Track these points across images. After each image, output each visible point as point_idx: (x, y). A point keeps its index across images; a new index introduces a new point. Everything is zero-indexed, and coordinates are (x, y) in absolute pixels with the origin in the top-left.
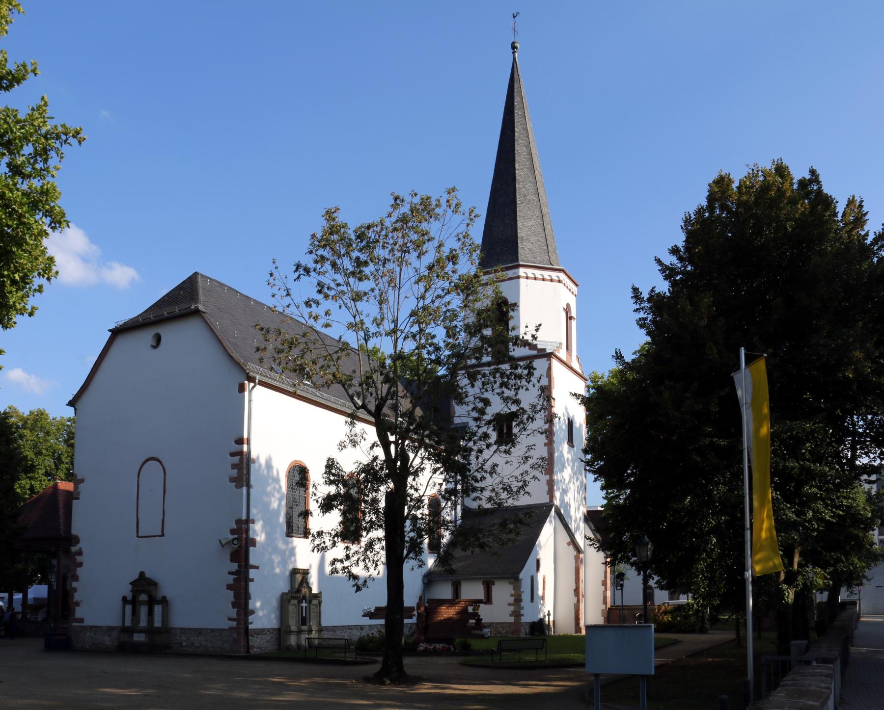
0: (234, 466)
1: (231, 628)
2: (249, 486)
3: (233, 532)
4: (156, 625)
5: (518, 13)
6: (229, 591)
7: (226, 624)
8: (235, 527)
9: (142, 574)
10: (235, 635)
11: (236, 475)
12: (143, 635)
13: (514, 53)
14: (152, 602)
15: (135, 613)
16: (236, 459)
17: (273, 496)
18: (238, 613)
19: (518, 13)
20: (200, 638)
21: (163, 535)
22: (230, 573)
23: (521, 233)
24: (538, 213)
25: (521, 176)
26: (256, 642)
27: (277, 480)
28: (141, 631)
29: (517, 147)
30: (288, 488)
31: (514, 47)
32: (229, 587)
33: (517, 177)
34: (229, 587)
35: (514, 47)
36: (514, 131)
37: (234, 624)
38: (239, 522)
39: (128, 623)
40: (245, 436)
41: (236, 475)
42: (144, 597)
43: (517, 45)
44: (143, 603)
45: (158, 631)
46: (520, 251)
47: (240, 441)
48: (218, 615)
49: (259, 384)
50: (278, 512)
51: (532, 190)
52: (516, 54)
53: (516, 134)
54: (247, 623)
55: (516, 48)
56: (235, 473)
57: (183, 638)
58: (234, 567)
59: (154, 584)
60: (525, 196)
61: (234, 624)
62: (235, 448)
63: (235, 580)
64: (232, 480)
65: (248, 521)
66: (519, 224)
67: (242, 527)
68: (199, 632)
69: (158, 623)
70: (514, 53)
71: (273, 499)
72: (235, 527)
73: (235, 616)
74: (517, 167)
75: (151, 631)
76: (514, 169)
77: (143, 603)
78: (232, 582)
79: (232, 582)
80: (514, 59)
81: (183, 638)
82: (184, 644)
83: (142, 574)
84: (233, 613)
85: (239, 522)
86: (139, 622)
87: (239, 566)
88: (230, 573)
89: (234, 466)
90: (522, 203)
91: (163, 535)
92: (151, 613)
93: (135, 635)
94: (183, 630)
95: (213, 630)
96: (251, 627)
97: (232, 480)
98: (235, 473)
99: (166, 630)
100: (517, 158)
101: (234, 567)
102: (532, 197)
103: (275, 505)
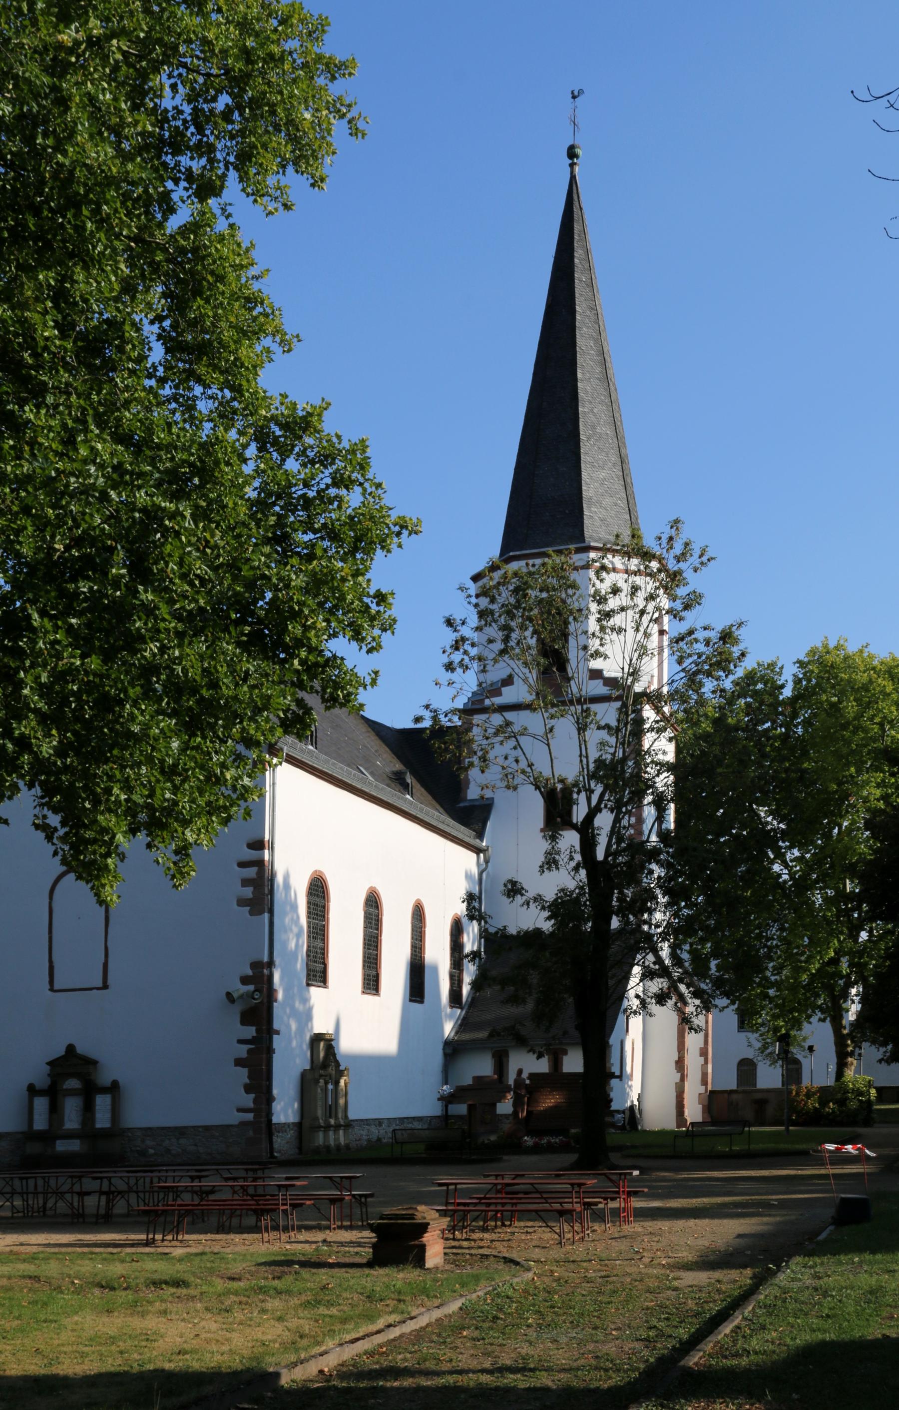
0: (245, 882)
1: (243, 1124)
2: (271, 912)
3: (245, 980)
4: (98, 1125)
5: (581, 92)
6: (238, 1068)
7: (235, 1118)
8: (250, 972)
9: (71, 1049)
10: (251, 1133)
11: (250, 896)
12: (77, 1142)
13: (572, 165)
14: (90, 1092)
15: (55, 1109)
16: (251, 872)
17: (291, 930)
18: (255, 1101)
19: (581, 92)
20: (183, 1141)
21: (105, 986)
22: (240, 1042)
23: (588, 491)
24: (615, 458)
25: (586, 392)
26: (283, 1143)
27: (294, 907)
28: (70, 1135)
29: (580, 341)
30: (309, 917)
31: (572, 153)
32: (239, 1062)
33: (581, 394)
34: (239, 1062)
35: (572, 153)
36: (573, 312)
37: (250, 1116)
38: (257, 966)
39: (40, 1123)
40: (267, 837)
41: (250, 896)
42: (73, 1083)
43: (579, 151)
44: (72, 1092)
45: (105, 1134)
46: (587, 522)
47: (258, 845)
48: (221, 1102)
49: (287, 761)
50: (295, 955)
51: (605, 417)
52: (577, 169)
53: (578, 317)
54: (269, 1113)
55: (577, 156)
56: (248, 892)
57: (149, 1142)
58: (250, 1032)
59: (91, 1063)
60: (593, 427)
61: (250, 1116)
62: (252, 855)
63: (249, 1051)
64: (242, 902)
65: (271, 964)
66: (584, 475)
67: (260, 976)
68: (181, 1132)
69: (102, 1120)
70: (572, 165)
71: (291, 936)
72: (250, 972)
73: (251, 1105)
74: (579, 375)
75: (88, 1133)
76: (575, 380)
77: (72, 1092)
78: (244, 1055)
79: (244, 1055)
80: (573, 178)
81: (149, 1142)
82: (151, 1151)
83: (71, 1049)
84: (248, 1100)
85: (257, 966)
86: (61, 1122)
87: (257, 1031)
88: (240, 1042)
89: (245, 882)
90: (589, 439)
91: (105, 986)
92: (88, 1108)
93: (58, 1142)
94: (149, 1132)
95: (207, 1128)
96: (275, 1120)
97: (242, 902)
98: (248, 892)
99: (115, 1132)
100: (580, 360)
101: (250, 1032)
102: (605, 430)
103: (292, 945)
